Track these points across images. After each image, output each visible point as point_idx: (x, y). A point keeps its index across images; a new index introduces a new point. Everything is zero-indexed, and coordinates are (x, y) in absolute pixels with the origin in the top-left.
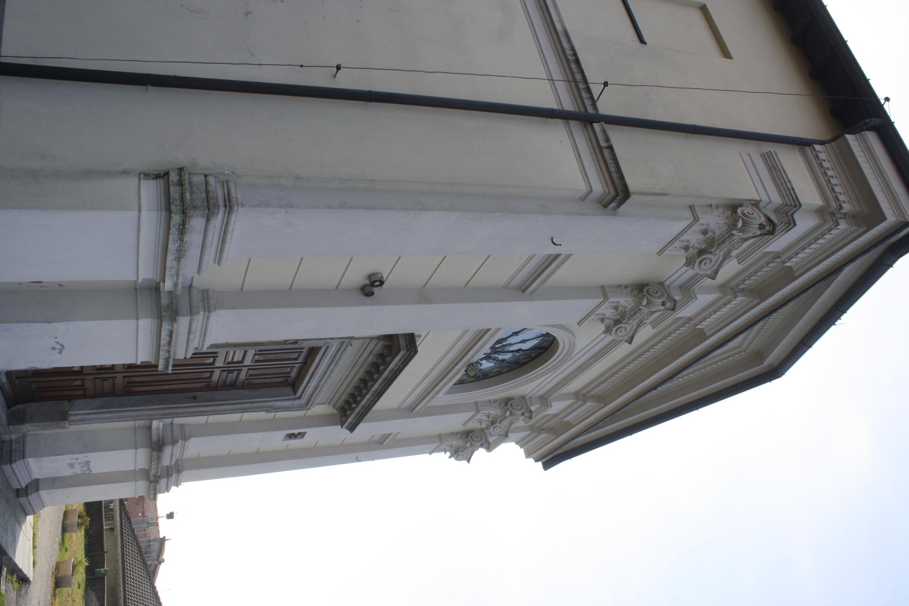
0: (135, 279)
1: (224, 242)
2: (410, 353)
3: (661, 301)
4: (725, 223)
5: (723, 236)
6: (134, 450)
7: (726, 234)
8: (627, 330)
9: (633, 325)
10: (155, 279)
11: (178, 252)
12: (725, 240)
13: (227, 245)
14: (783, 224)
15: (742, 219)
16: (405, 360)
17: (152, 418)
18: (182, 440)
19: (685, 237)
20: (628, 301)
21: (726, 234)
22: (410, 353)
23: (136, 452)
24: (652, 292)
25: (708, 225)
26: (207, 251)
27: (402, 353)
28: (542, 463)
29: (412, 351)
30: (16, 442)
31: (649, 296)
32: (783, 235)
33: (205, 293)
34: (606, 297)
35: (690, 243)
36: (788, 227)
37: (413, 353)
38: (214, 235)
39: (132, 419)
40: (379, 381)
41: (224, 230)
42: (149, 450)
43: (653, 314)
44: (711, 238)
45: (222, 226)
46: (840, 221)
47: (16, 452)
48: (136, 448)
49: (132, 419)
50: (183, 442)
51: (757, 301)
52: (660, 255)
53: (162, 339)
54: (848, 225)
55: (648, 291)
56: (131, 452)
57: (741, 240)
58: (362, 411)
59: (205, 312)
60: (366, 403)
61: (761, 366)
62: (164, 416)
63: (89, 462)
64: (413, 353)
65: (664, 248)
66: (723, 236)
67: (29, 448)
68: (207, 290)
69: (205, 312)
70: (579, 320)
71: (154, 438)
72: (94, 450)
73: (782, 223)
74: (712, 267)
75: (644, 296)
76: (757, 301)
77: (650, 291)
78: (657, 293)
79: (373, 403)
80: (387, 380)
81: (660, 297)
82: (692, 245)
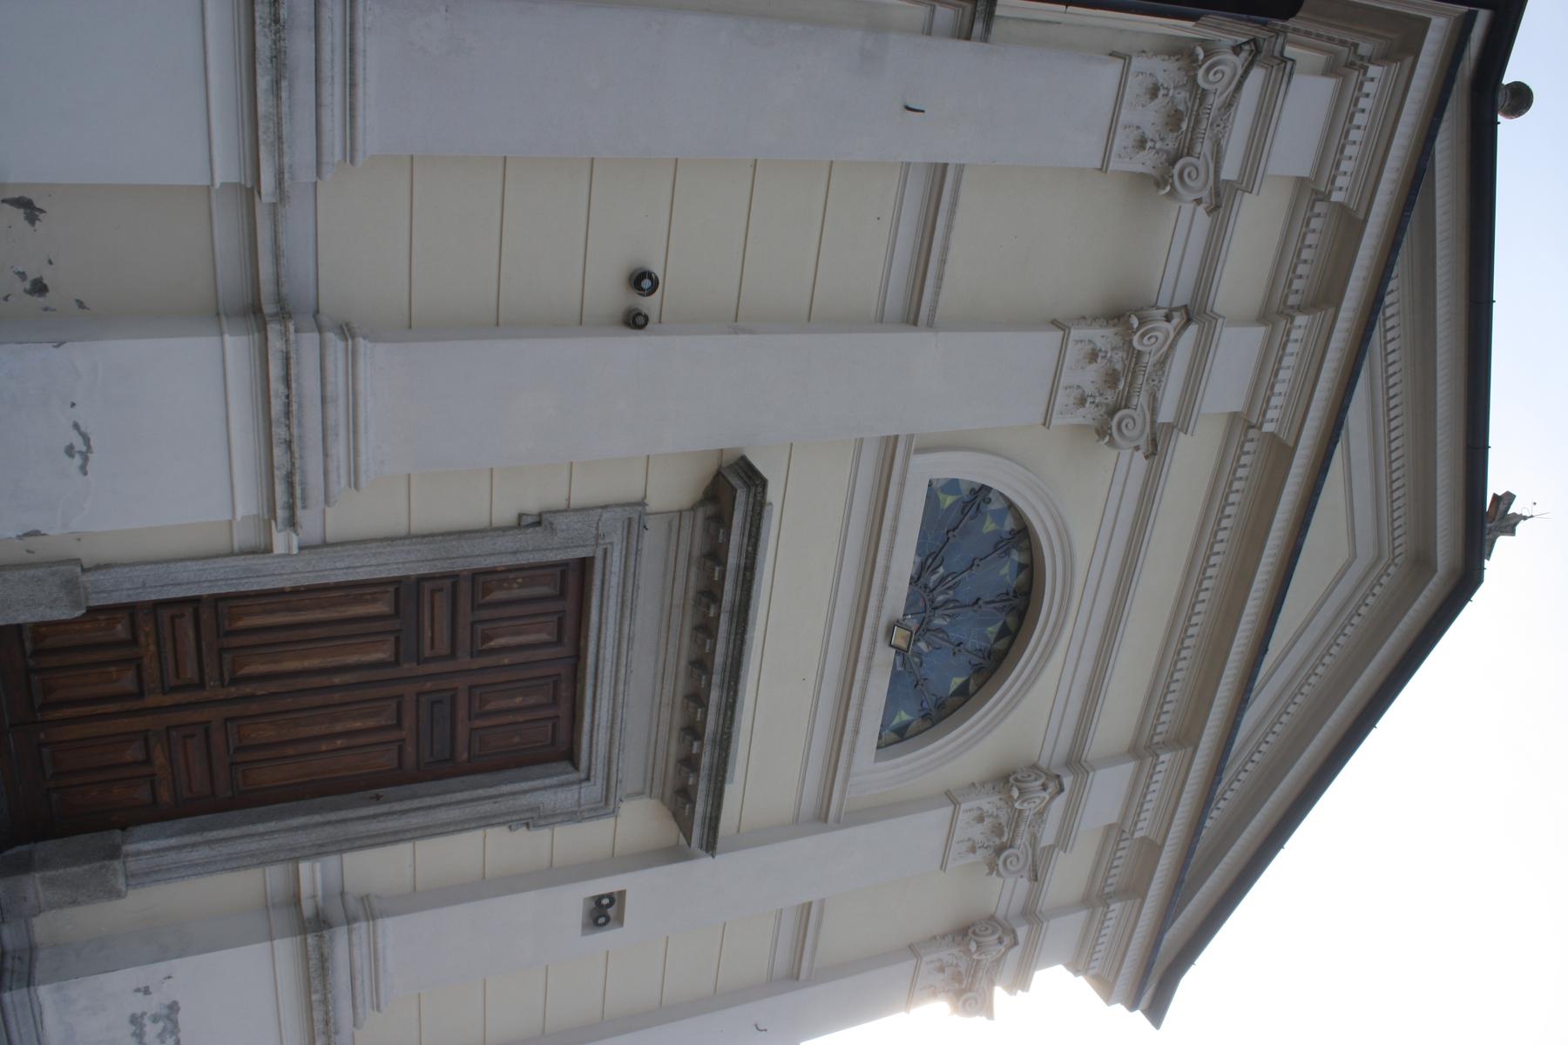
0: (229, 517)
1: (353, 85)
2: (756, 490)
3: (1039, 783)
4: (1116, 334)
5: (1013, 818)
6: (267, 944)
7: (1193, 105)
8: (1159, 341)
9: (1142, 406)
10: (261, 514)
11: (274, 60)
12: (1198, 114)
13: (360, 91)
14: (1275, 68)
15: (1017, 786)
16: (751, 525)
17: (298, 855)
18: (368, 920)
19: (958, 835)
20: (953, 955)
21: (1193, 105)
22: (756, 490)
23: (272, 946)
24: (980, 930)
25: (980, 809)
26: (326, 90)
27: (741, 496)
28: (1143, 1011)
29: (757, 486)
30: (13, 958)
31: (976, 938)
32: (1286, 93)
33: (364, 899)
34: (956, 803)
35: (974, 842)
36: (1285, 68)
37: (760, 489)
38: (333, 116)
39: (255, 861)
40: (724, 619)
41: (350, 72)
42: (298, 938)
43: (1164, 366)
44: (1173, 112)
45: (345, 62)
46: (1158, 752)
47: (13, 972)
48: (272, 939)
49: (255, 861)
50: (371, 923)
51: (1409, 60)
52: (1049, 425)
53: (272, 393)
54: (1383, 66)
55: (974, 933)
56: (259, 950)
57: (1037, 816)
58: (716, 755)
59: (347, 340)
60: (717, 724)
61: (1436, 579)
62: (319, 851)
63: (174, 1007)
64: (760, 489)
65: (1058, 363)
66: (1013, 818)
67: (40, 970)
68: (367, 896)
69: (347, 340)
70: (939, 864)
71: (308, 908)
72: (183, 953)
73: (1272, 67)
74: (1142, 432)
75: (971, 938)
76: (1331, 311)
77: (977, 930)
78: (987, 929)
79: (719, 785)
80: (715, 767)
81: (993, 933)
82: (980, 845)
